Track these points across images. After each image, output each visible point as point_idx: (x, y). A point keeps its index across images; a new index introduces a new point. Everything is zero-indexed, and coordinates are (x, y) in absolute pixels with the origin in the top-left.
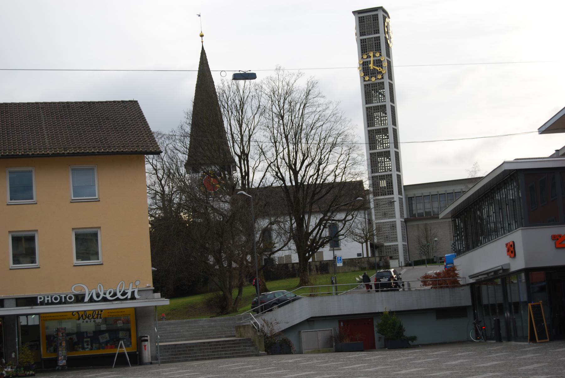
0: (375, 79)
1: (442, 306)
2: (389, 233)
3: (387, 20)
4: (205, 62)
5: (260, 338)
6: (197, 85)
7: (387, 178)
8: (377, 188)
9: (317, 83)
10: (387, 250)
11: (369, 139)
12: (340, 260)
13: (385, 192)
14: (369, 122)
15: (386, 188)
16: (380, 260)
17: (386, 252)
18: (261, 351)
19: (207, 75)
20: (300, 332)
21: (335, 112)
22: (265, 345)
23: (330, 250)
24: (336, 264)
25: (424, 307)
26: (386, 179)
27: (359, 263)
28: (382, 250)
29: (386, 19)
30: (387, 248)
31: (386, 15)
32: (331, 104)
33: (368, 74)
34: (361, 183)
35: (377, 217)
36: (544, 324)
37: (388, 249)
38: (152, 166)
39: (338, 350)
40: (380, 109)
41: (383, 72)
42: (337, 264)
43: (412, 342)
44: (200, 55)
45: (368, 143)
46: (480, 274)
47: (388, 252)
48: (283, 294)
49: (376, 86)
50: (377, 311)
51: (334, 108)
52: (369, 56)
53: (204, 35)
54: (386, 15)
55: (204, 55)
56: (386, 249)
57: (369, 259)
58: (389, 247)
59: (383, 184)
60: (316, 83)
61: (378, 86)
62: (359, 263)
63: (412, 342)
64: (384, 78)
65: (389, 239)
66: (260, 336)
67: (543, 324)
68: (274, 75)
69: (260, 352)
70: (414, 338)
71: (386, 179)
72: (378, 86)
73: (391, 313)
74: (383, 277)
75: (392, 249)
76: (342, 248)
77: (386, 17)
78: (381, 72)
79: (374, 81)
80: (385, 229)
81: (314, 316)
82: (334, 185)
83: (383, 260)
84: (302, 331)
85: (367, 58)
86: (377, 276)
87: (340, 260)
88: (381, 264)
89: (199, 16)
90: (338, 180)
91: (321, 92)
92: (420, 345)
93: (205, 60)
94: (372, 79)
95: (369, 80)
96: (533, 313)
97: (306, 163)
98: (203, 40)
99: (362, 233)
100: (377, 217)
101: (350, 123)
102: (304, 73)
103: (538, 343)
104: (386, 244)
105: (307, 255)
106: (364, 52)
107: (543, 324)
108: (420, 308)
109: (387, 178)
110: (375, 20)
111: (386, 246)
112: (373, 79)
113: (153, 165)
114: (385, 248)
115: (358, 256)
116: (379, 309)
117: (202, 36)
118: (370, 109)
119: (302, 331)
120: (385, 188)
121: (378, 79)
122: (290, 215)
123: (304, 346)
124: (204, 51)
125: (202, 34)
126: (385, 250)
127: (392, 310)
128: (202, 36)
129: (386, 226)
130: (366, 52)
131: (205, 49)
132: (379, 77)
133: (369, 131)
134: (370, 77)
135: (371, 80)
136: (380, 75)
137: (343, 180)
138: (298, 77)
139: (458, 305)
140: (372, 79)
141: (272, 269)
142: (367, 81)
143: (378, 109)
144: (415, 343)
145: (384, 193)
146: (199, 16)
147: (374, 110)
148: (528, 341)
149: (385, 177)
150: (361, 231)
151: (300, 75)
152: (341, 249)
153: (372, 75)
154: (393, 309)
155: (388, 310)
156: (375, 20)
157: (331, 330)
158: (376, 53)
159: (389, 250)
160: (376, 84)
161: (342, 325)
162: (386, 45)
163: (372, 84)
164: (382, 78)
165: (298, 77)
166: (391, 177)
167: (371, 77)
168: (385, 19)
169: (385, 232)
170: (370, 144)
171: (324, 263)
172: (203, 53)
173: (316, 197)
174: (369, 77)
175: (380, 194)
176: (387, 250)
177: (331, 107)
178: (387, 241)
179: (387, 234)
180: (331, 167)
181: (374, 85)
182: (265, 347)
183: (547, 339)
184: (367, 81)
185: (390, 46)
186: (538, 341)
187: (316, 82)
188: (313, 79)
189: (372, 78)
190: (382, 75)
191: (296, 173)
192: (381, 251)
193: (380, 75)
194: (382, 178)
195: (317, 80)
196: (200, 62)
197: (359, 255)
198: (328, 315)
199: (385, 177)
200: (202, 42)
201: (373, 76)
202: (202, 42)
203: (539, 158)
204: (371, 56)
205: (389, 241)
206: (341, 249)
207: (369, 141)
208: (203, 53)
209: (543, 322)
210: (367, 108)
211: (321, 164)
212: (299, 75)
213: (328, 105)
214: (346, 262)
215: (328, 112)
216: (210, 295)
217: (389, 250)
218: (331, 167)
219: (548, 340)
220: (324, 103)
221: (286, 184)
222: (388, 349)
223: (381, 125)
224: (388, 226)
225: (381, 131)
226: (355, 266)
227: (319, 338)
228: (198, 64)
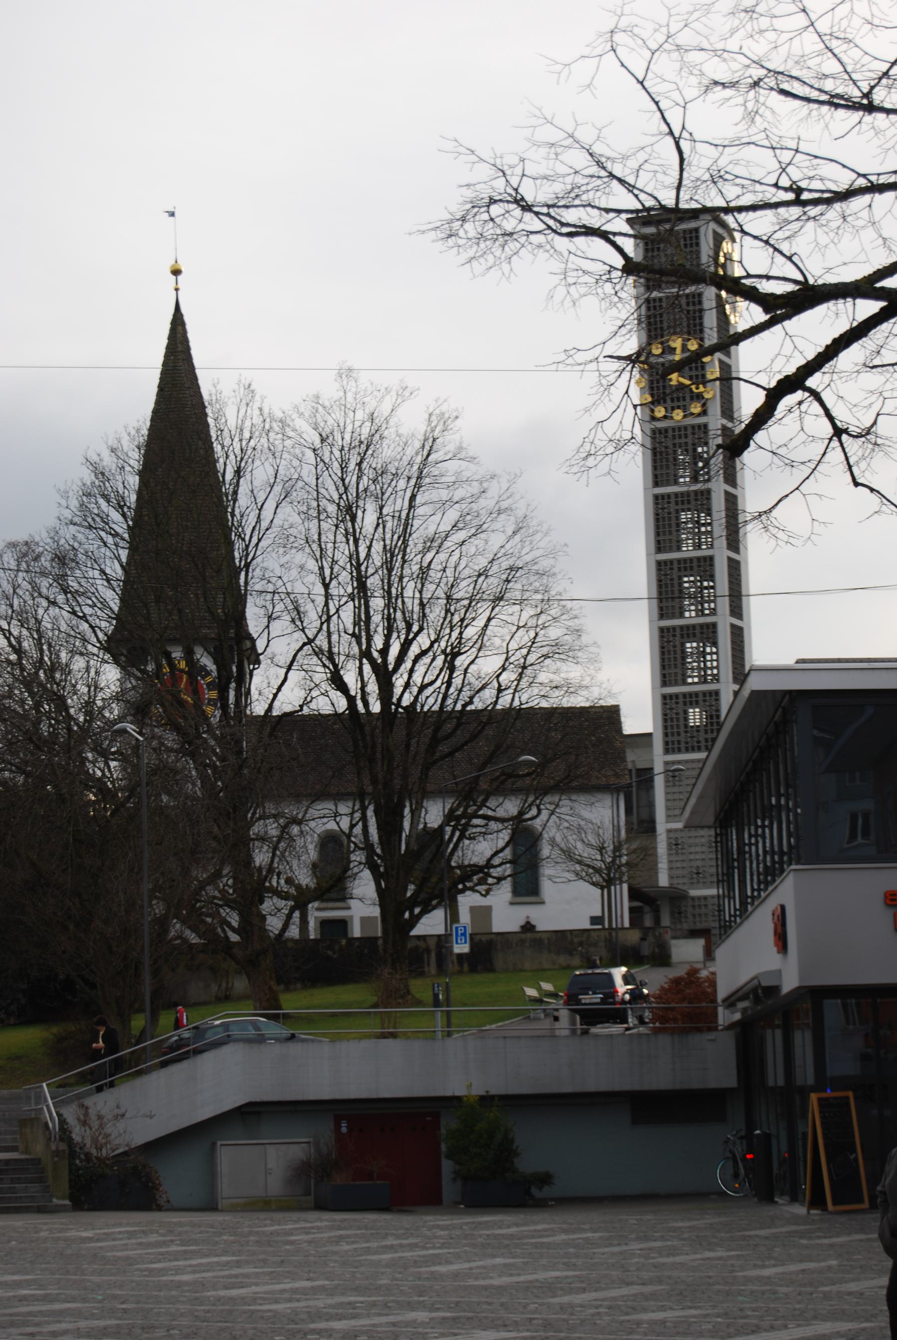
0: (682, 414)
1: (646, 1087)
2: (703, 859)
3: (726, 246)
4: (180, 348)
5: (56, 1159)
6: (155, 412)
7: (705, 701)
8: (675, 730)
9: (457, 417)
10: (697, 911)
11: (660, 586)
12: (462, 934)
13: (698, 742)
14: (661, 538)
15: (702, 729)
16: (643, 939)
17: (694, 916)
18: (57, 1198)
19: (186, 385)
20: (214, 1145)
21: (503, 505)
22: (70, 1181)
23: (512, 903)
24: (452, 947)
25: (591, 1086)
26: (701, 703)
27: (581, 944)
28: (683, 909)
29: (724, 244)
30: (697, 903)
31: (720, 230)
32: (495, 482)
33: (665, 402)
34: (612, 715)
35: (671, 813)
36: (856, 1159)
37: (700, 906)
38: (8, 639)
39: (321, 1206)
40: (693, 502)
41: (706, 396)
42: (455, 946)
43: (540, 1189)
44: (168, 326)
45: (655, 596)
46: (737, 996)
47: (700, 915)
48: (257, 1028)
49: (686, 436)
50: (449, 1093)
51: (502, 492)
52: (669, 347)
53: (183, 269)
54: (720, 230)
55: (180, 328)
56: (693, 906)
57: (610, 934)
58: (703, 902)
59: (695, 717)
60: (453, 417)
61: (690, 436)
62: (581, 944)
63: (540, 1189)
64: (710, 412)
65: (704, 878)
66: (57, 1153)
67: (852, 1157)
68: (330, 391)
69: (55, 1200)
70: (545, 1179)
71: (701, 703)
72: (690, 436)
73: (486, 1100)
74: (589, 989)
75: (710, 907)
76: (547, 900)
77: (724, 239)
78: (699, 396)
79: (678, 421)
80: (692, 850)
81: (253, 1099)
82: (489, 716)
83: (651, 939)
84: (219, 1143)
85: (663, 353)
86: (572, 984)
87: (464, 934)
88: (646, 950)
89: (172, 214)
90: (505, 701)
91: (464, 445)
92: (552, 1199)
93: (182, 343)
94: (674, 415)
95: (665, 417)
96: (822, 1124)
97: (414, 650)
98: (180, 286)
99: (599, 857)
100: (671, 813)
101: (547, 539)
102: (418, 389)
103: (831, 1213)
104: (694, 893)
105: (407, 915)
106: (656, 338)
107: (852, 1157)
108: (578, 1088)
109: (705, 701)
110: (691, 245)
111: (693, 898)
112: (678, 415)
113: (12, 639)
114: (690, 902)
115: (592, 924)
116: (454, 1087)
117: (176, 272)
118: (666, 500)
119: (219, 1143)
120: (698, 731)
121: (692, 414)
122: (361, 796)
123: (226, 1188)
124: (182, 315)
125: (177, 267)
126: (690, 909)
127: (493, 1092)
128: (176, 272)
129: (697, 840)
130: (662, 337)
131: (184, 310)
132: (696, 408)
133: (659, 563)
134: (669, 409)
135: (672, 418)
136: (699, 405)
137: (516, 703)
138: (399, 400)
139: (696, 1085)
140: (674, 415)
141: (330, 953)
142: (658, 420)
143: (689, 502)
144: (547, 1192)
145: (695, 744)
146: (172, 214)
147: (677, 503)
148: (807, 1204)
149: (701, 698)
150: (593, 852)
151: (407, 393)
152: (543, 903)
153: (676, 404)
154: (497, 1088)
155: (478, 1090)
156: (691, 245)
157: (309, 1143)
158: (689, 340)
159: (703, 910)
160: (686, 428)
161: (344, 1130)
162: (718, 318)
163: (674, 429)
164: (704, 413)
165: (399, 400)
166: (717, 700)
167: (673, 409)
168: (721, 243)
169: (692, 857)
170: (660, 600)
171: (480, 941)
172: (178, 323)
173: (443, 748)
174: (666, 408)
175: (683, 746)
176: (697, 911)
177: (494, 490)
178: (698, 882)
179: (699, 863)
180: (488, 665)
181: (680, 431)
182: (71, 1187)
183: (861, 1201)
184: (658, 420)
185: (733, 322)
186: (830, 1207)
187: (455, 414)
188: (444, 408)
189: (677, 411)
190: (704, 405)
191: (384, 677)
192: (680, 913)
193: (699, 405)
194: (692, 699)
195: (457, 410)
196: (168, 348)
197: (594, 920)
198: (300, 1098)
199: (701, 698)
200: (177, 290)
201: (679, 408)
202: (177, 290)
203: (839, 661)
204: (675, 349)
205: (704, 883)
206: (543, 903)
207: (660, 593)
208: (178, 323)
209: (854, 1150)
210: (656, 497)
211: (459, 654)
212: (404, 393)
213: (485, 485)
214: (546, 942)
215: (486, 503)
216: (55, 1030)
217: (703, 910)
218: (488, 665)
219: (866, 1205)
220: (476, 477)
221: (371, 708)
222: (467, 1206)
223: (699, 547)
224: (703, 840)
225: (695, 564)
226: (571, 954)
227: (270, 1166)
228: (162, 351)
